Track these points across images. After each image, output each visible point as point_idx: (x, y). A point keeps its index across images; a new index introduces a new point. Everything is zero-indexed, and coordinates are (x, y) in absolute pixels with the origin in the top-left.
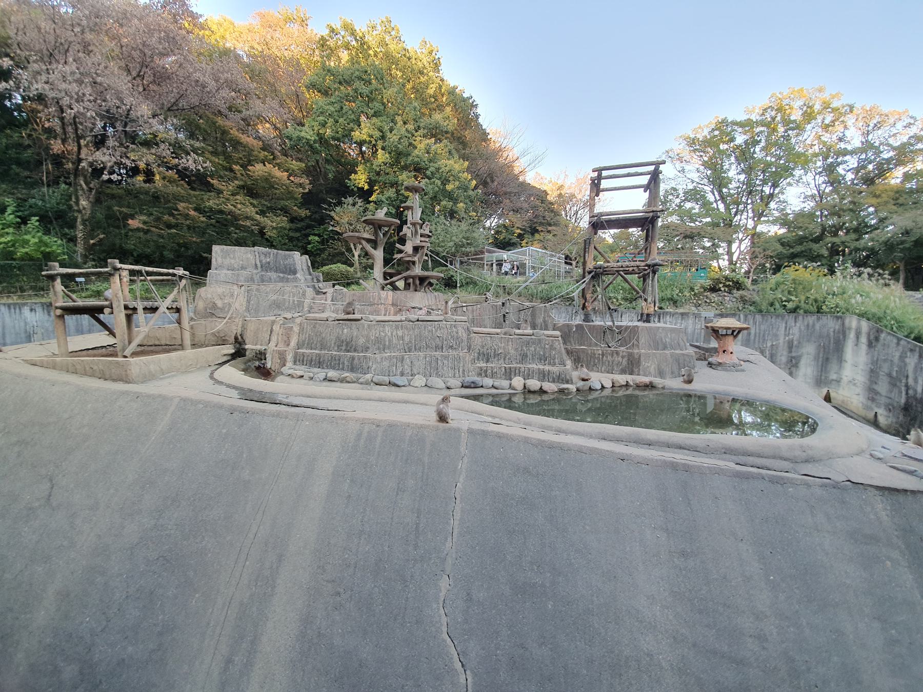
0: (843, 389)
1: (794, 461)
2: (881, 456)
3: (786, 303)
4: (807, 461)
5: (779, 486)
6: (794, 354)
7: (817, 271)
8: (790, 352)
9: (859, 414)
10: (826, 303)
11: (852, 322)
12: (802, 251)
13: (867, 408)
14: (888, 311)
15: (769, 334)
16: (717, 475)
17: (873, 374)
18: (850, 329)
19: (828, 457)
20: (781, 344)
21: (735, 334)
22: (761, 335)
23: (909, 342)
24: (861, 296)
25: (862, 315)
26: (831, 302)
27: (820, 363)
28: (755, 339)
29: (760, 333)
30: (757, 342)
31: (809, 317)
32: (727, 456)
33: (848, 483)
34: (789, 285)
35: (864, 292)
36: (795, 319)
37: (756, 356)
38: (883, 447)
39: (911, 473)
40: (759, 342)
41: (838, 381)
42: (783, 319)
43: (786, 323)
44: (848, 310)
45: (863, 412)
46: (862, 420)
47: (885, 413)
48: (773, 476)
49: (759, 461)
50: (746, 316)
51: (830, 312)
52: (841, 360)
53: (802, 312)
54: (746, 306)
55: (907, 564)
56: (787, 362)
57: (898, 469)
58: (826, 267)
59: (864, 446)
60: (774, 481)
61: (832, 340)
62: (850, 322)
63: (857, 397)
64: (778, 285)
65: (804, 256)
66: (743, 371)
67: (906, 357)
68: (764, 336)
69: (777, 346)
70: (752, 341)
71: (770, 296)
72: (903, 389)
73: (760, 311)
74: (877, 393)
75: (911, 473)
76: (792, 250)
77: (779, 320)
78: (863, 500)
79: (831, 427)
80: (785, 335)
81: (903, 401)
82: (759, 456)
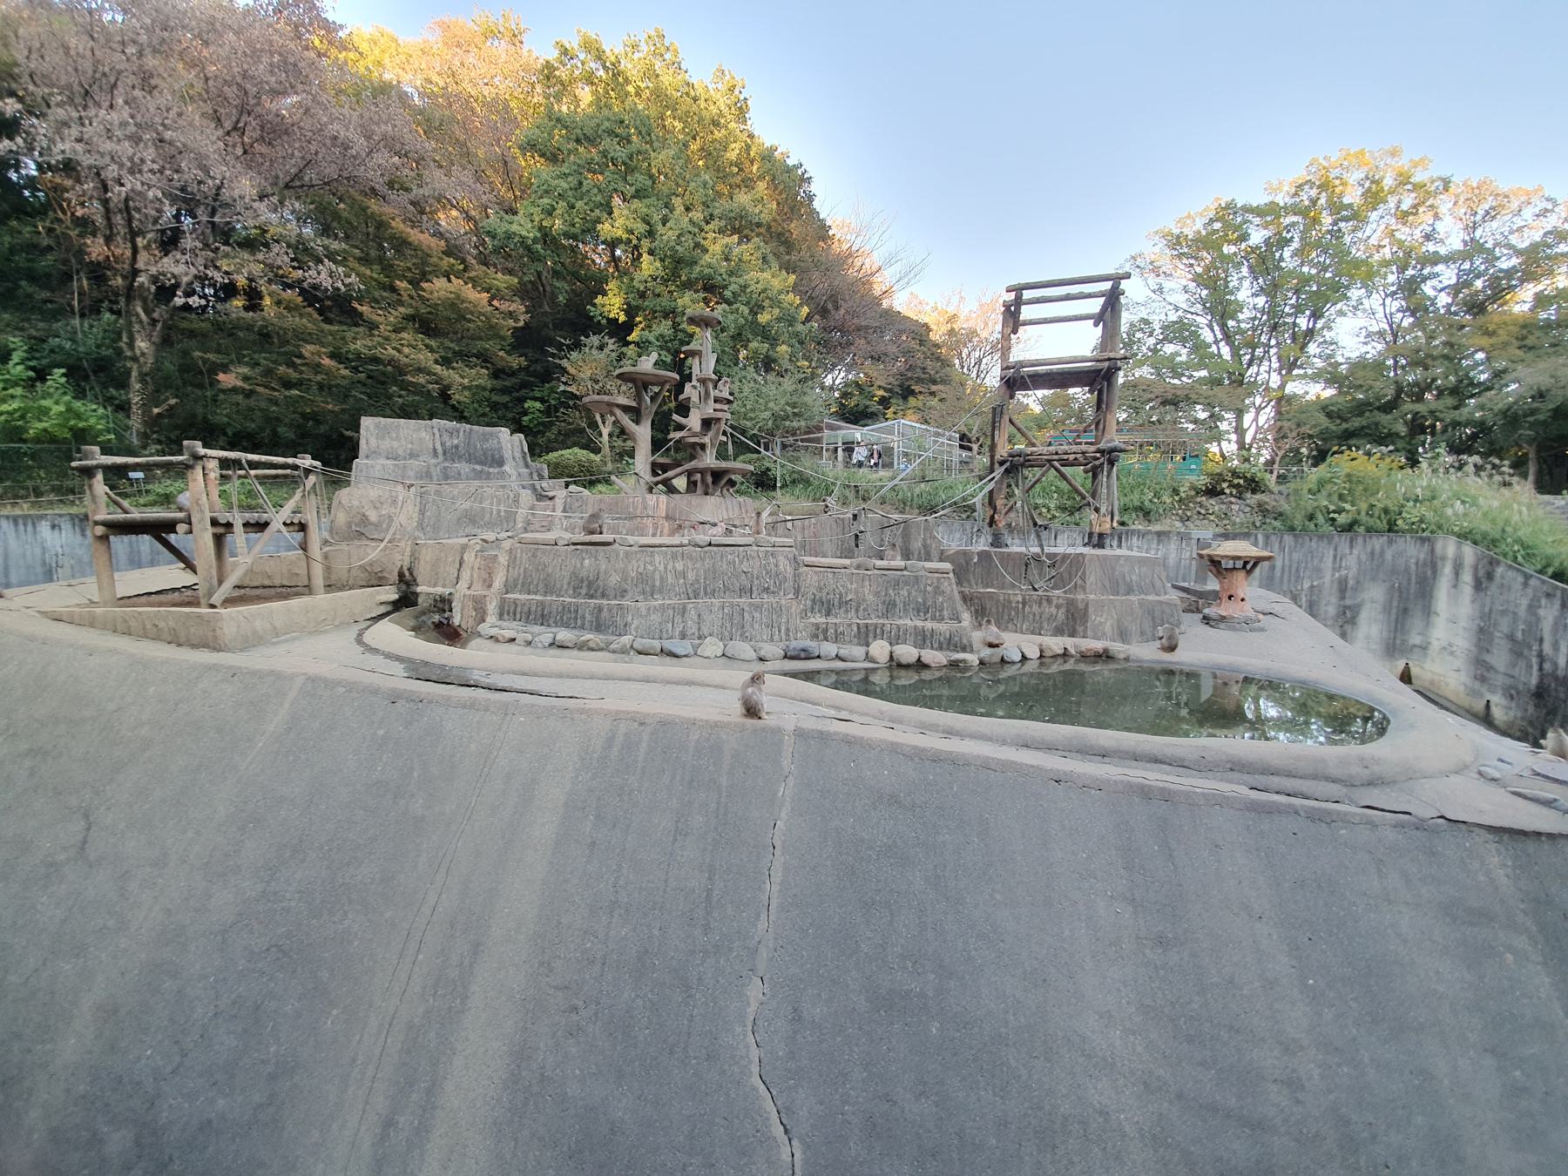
0: (1433, 661)
1: (1348, 783)
2: (1497, 775)
3: (1336, 516)
4: (1371, 784)
5: (1324, 825)
6: (1348, 602)
7: (1388, 460)
8: (1343, 598)
9: (1460, 703)
10: (1404, 515)
11: (1448, 547)
12: (1363, 427)
13: (1474, 693)
14: (1509, 529)
15: (1306, 568)
16: (1217, 807)
17: (1483, 636)
18: (1444, 558)
19: (1407, 776)
20: (1327, 585)
21: (1248, 567)
22: (1293, 570)
23: (1544, 582)
24: (1463, 502)
25: (1464, 536)
26: (1412, 513)
27: (1393, 617)
28: (1282, 577)
29: (1290, 566)
30: (1285, 581)
31: (1374, 539)
32: (1236, 775)
33: (1441, 820)
34: (1341, 485)
35: (1467, 496)
36: (1351, 542)
37: (1284, 605)
38: (1501, 760)
39: (1548, 803)
40: (1289, 581)
41: (1424, 648)
42: (1330, 542)
43: (1336, 550)
44: (1440, 527)
45: (1465, 701)
46: (1464, 713)
47: (1503, 702)
48: (1313, 808)
49: (1290, 784)
50: (1267, 537)
51: (1411, 531)
52: (1428, 612)
53: (1362, 530)
54: (1268, 521)
55: (1541, 959)
56: (1338, 616)
57: (1525, 797)
58: (1403, 453)
59: (1469, 759)
60: (1314, 817)
61: (1413, 577)
62: (1444, 547)
63: (1455, 675)
64: (1321, 484)
65: (1367, 434)
66: (1262, 630)
67: (1540, 607)
68: (1298, 570)
69: (1320, 588)
70: (1277, 580)
71: (1308, 503)
72: (1535, 661)
73: (1292, 529)
74: (1490, 668)
75: (1548, 803)
76: (1345, 426)
77: (1323, 544)
78: (1466, 849)
79: (1412, 726)
80: (1334, 569)
81: (1534, 681)
82: (1290, 775)
